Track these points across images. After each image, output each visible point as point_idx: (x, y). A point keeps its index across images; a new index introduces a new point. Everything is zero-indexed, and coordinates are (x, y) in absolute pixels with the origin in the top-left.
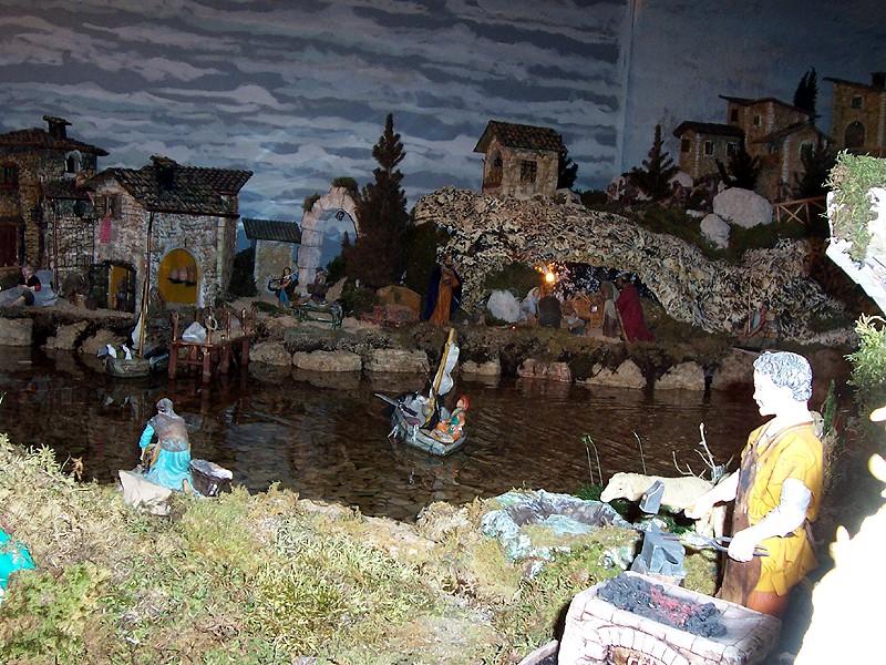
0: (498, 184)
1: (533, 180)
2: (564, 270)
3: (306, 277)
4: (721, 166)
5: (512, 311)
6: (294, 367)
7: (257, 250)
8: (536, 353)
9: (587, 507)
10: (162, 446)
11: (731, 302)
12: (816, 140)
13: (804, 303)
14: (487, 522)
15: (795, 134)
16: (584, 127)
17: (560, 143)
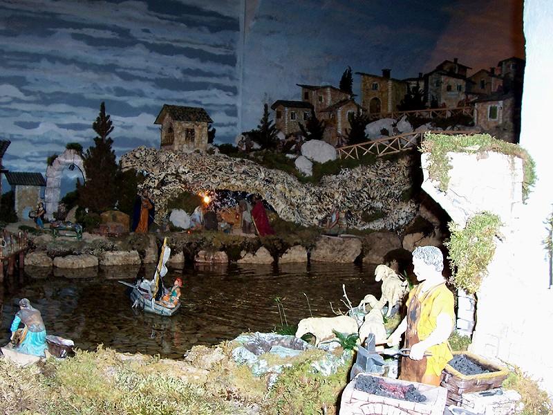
0: (171, 144)
1: (193, 141)
2: (214, 194)
3: (52, 208)
4: (301, 126)
5: (185, 221)
6: (54, 267)
7: (16, 192)
8: (205, 247)
9: (287, 339)
10: (29, 329)
11: (317, 208)
12: (356, 109)
13: (359, 206)
14: (235, 354)
15: (344, 106)
16: (216, 105)
17: (208, 117)
